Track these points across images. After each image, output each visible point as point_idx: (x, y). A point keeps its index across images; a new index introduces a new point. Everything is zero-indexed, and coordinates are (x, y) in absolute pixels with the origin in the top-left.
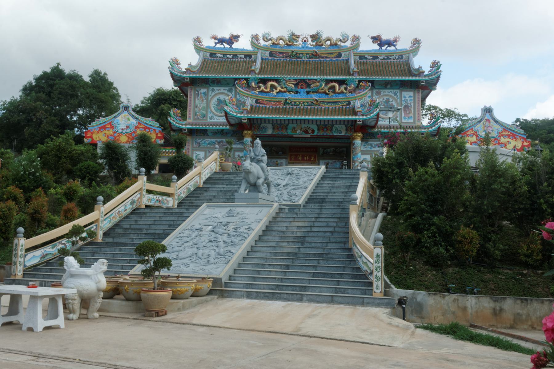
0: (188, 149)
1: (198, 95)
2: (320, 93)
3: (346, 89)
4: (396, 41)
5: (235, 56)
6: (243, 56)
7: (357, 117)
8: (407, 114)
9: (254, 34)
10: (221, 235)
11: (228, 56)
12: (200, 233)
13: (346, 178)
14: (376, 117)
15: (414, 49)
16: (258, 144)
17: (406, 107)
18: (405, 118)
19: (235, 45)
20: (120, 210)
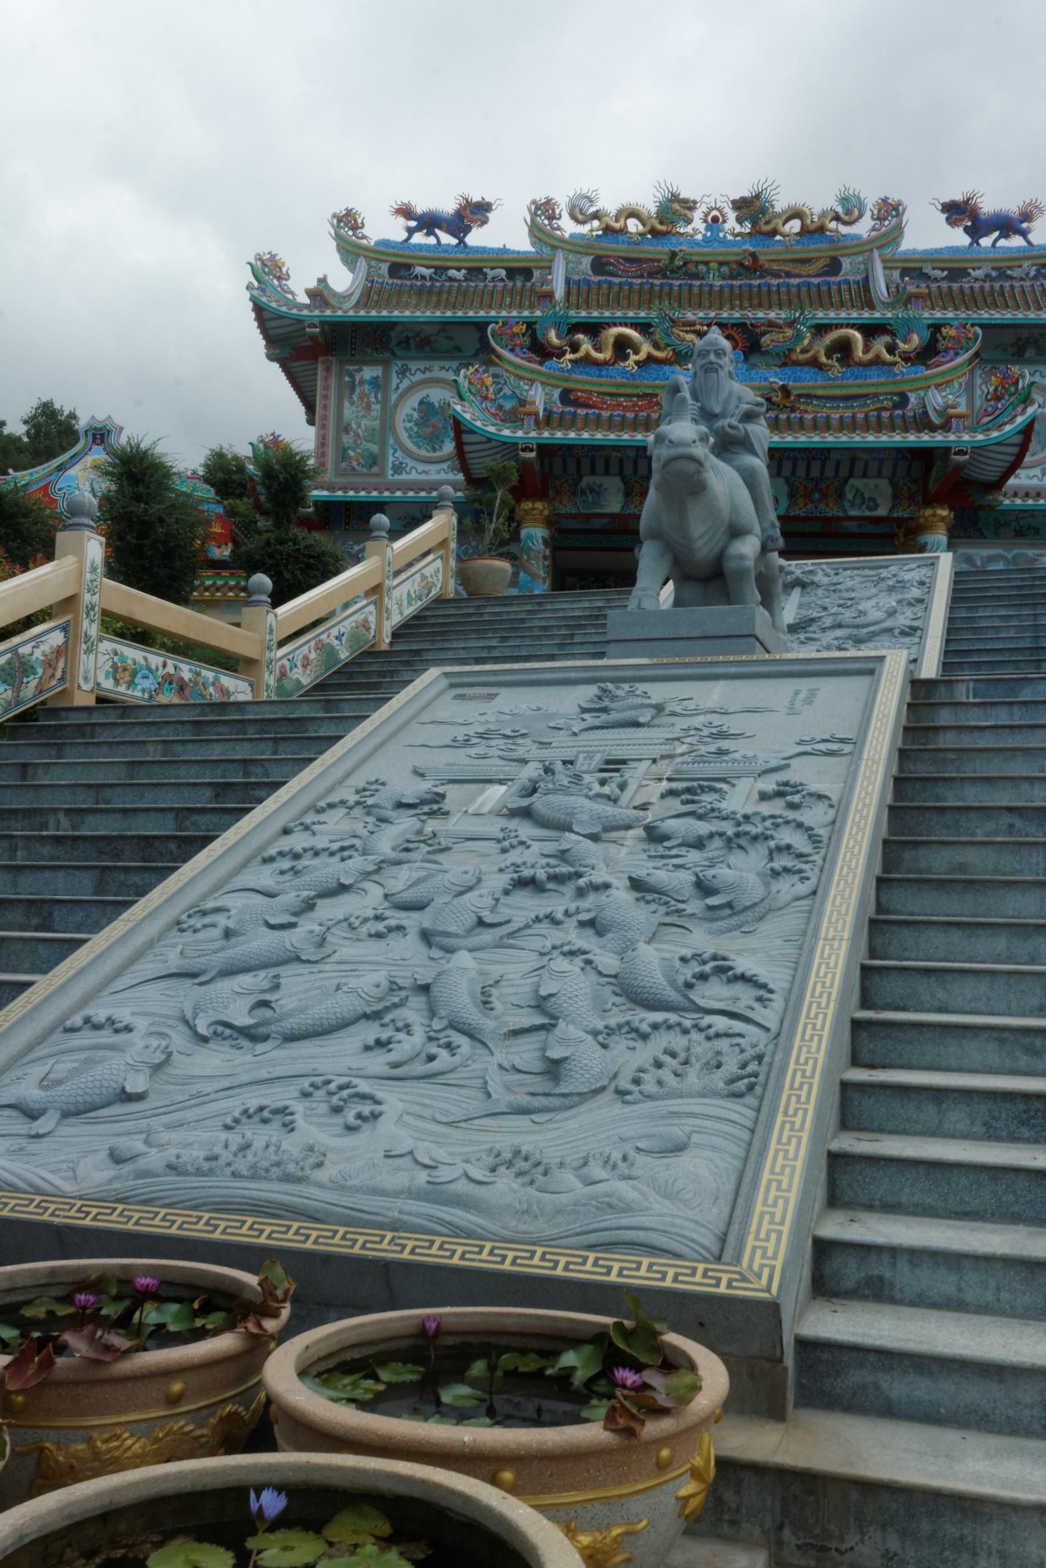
1: (352, 389)
2: (797, 363)
3: (891, 349)
4: (1027, 216)
5: (475, 272)
6: (503, 273)
7: (952, 437)
9: (541, 197)
10: (595, 838)
11: (452, 273)
12: (432, 825)
14: (1018, 439)
16: (720, 353)
19: (476, 238)
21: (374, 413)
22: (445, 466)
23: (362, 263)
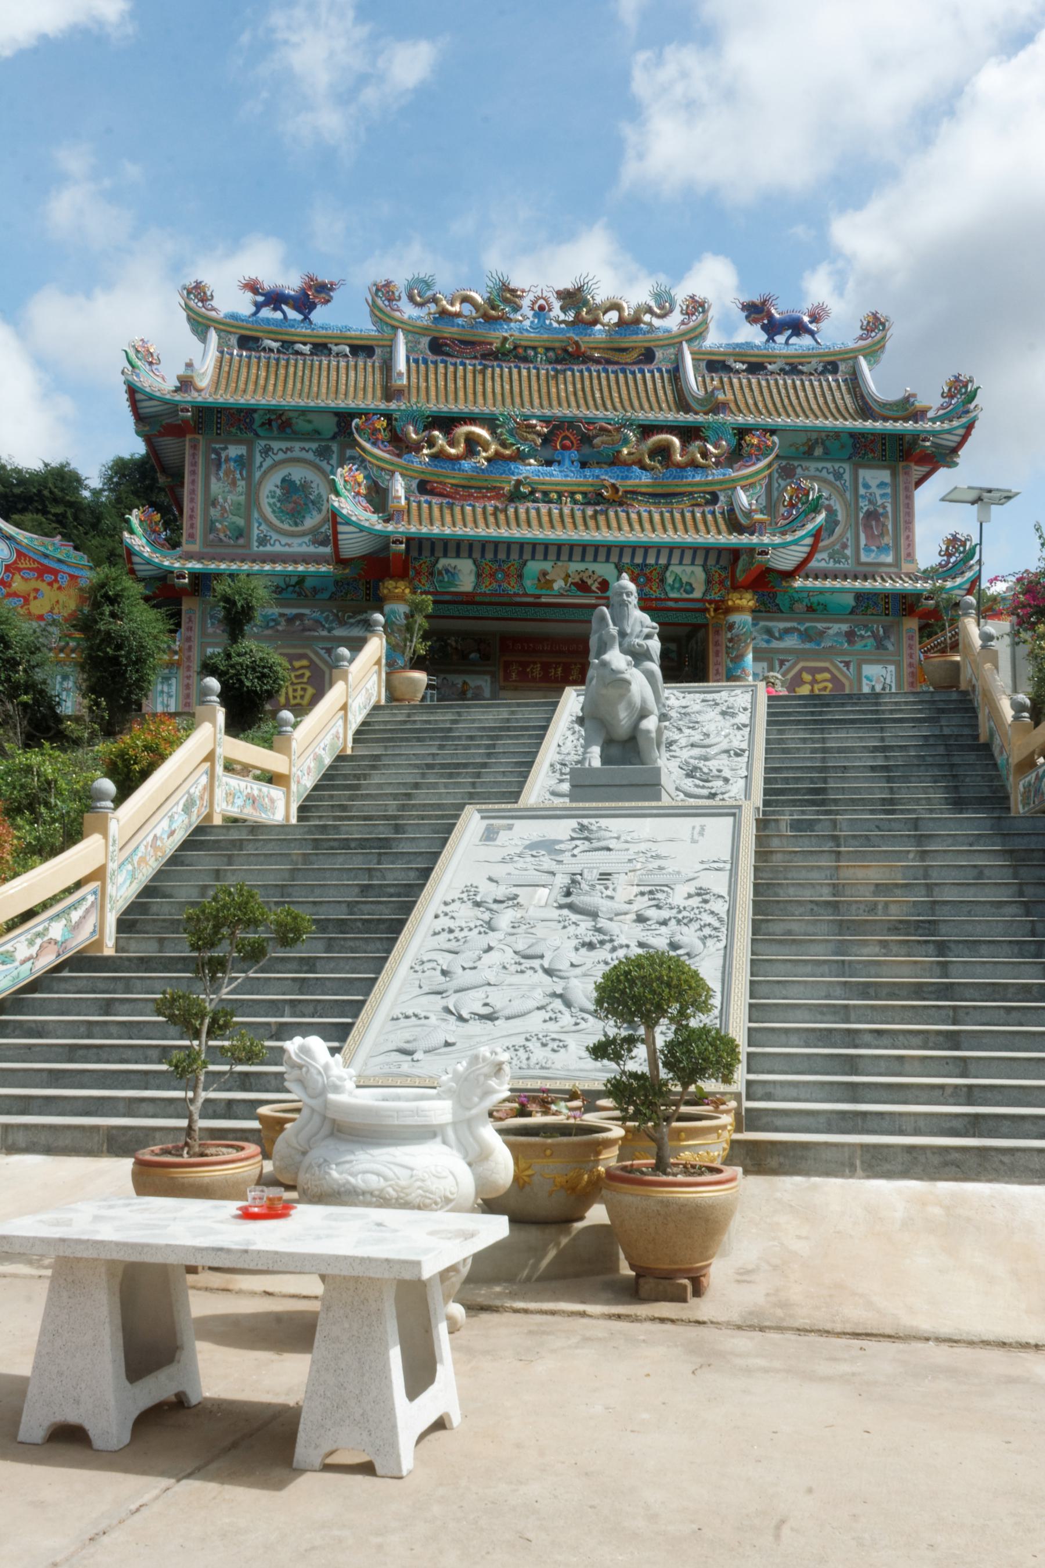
0: (189, 639)
1: (219, 466)
6: (347, 349)
8: (873, 535)
10: (611, 919)
11: (299, 347)
13: (853, 721)
15: (870, 346)
16: (629, 594)
17: (872, 515)
18: (867, 549)
19: (320, 315)
20: (158, 831)
21: (239, 489)
22: (306, 539)
23: (213, 336)
